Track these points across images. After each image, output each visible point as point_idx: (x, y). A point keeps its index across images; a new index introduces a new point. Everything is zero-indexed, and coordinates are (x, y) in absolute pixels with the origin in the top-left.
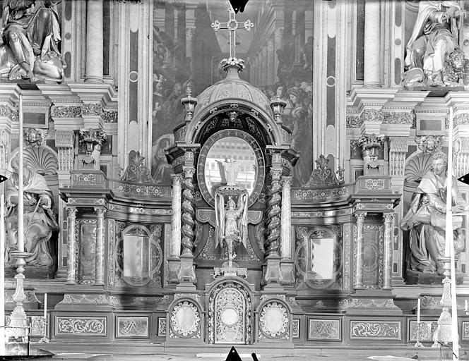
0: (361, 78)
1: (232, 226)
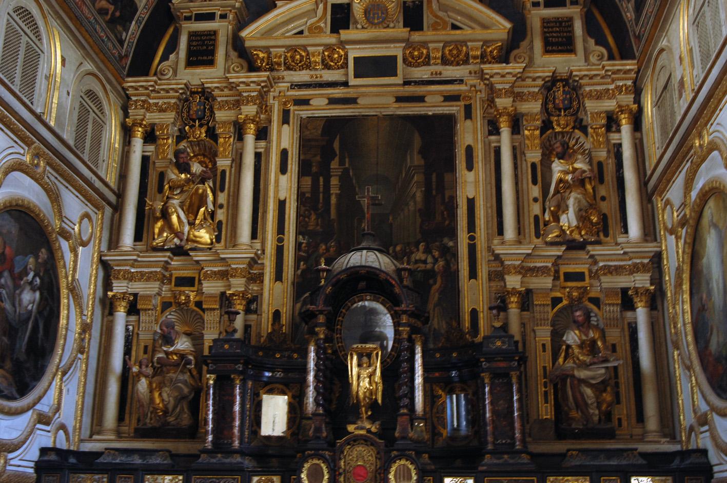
0: (501, 231)
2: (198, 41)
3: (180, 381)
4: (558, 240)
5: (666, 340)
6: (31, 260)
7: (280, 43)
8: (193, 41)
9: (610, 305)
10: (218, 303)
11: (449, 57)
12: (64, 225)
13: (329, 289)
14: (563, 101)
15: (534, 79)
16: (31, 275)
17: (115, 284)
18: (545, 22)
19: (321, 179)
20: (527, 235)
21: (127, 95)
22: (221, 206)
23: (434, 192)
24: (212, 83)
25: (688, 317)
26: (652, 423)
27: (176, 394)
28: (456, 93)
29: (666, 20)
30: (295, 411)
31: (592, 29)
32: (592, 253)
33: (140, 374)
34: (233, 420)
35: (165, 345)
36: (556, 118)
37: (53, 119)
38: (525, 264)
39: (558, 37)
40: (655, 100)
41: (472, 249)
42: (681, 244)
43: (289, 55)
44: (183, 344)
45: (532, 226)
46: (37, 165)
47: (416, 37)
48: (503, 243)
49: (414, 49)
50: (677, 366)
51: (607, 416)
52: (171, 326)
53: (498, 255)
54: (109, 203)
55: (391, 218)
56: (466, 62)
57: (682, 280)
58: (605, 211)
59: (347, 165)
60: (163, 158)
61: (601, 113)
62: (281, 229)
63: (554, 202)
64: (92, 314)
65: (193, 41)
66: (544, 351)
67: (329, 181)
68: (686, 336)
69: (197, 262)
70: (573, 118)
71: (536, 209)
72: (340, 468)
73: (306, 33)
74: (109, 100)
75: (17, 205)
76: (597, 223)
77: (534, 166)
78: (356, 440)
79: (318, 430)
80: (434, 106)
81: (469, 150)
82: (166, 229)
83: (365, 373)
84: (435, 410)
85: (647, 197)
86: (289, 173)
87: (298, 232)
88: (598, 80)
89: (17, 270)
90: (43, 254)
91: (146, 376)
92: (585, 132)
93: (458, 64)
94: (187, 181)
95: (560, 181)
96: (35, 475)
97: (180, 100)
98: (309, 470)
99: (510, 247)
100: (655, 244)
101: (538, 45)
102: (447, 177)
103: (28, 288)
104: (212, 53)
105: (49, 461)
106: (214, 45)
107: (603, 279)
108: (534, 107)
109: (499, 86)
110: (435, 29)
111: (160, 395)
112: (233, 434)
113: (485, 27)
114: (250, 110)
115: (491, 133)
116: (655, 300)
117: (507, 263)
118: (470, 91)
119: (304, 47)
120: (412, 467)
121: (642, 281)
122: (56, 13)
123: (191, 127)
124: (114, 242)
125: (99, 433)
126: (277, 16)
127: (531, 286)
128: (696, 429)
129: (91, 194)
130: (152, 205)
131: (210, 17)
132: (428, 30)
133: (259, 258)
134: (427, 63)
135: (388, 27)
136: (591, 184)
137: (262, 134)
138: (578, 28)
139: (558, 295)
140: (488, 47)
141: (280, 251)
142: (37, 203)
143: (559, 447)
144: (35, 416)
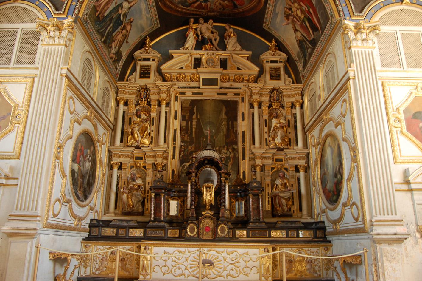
0: (254, 143)
2: (144, 69)
3: (138, 195)
4: (274, 147)
5: (310, 183)
6: (89, 151)
7: (175, 71)
8: (142, 69)
9: (291, 170)
10: (152, 167)
11: (236, 79)
12: (98, 138)
13: (197, 164)
14: (276, 97)
15: (267, 89)
16: (89, 156)
17: (113, 158)
18: (271, 68)
19: (189, 122)
20: (263, 145)
21: (117, 88)
22: (152, 131)
23: (230, 128)
24: (150, 85)
25: (319, 176)
26: (305, 212)
27: (137, 200)
28: (238, 93)
29: (314, 73)
30: (182, 207)
31: (287, 72)
32: (286, 152)
33: (123, 193)
34: (161, 210)
35: (133, 182)
36: (274, 103)
37: (96, 99)
38: (262, 156)
39: (275, 74)
40: (309, 99)
41: (244, 150)
42: (317, 151)
43: (178, 76)
44: (139, 182)
45: (265, 142)
46: (91, 116)
47: (225, 72)
48: (254, 148)
49: (224, 76)
50: (314, 193)
51: (290, 209)
52: (135, 175)
53: (253, 152)
54: (111, 129)
55: (214, 137)
56: (242, 82)
57: (318, 163)
58: (290, 137)
59: (199, 117)
60: (131, 112)
61: (290, 102)
62: (175, 140)
63: (273, 134)
64: (106, 170)
65: (142, 69)
66: (268, 186)
67: (192, 123)
68: (318, 183)
69: (144, 151)
70: (280, 104)
71: (266, 136)
72: (200, 227)
73: (184, 68)
74: (112, 90)
75: (86, 131)
76: (288, 142)
77: (266, 120)
78: (206, 217)
79: (192, 214)
80: (230, 97)
81: (243, 114)
82: (133, 139)
83: (208, 194)
84: (231, 207)
85: (305, 133)
86: (177, 120)
87: (181, 141)
88: (289, 90)
89: (85, 155)
90: (92, 148)
91: (126, 193)
92: (284, 109)
93: (239, 82)
94: (141, 121)
95: (275, 126)
96: (89, 229)
97: (137, 90)
98: (190, 228)
99: (257, 149)
100: (307, 150)
101: (268, 76)
102: (235, 123)
103: (88, 161)
104: (149, 73)
105: (94, 224)
106: (150, 71)
107: (289, 161)
108: (266, 99)
109: (254, 91)
110: (232, 69)
111: (131, 200)
112: (161, 215)
113: (250, 69)
114: (163, 96)
115: (250, 108)
116: (307, 169)
117: (256, 155)
118: (243, 92)
119: (184, 74)
120: (226, 227)
121: (303, 162)
122: (98, 60)
123: (141, 101)
124: (113, 143)
125: (107, 213)
126: (174, 61)
127: (264, 163)
128: (321, 214)
129: (106, 126)
130: (127, 130)
131: (148, 60)
132: (229, 69)
133: (167, 150)
134: (228, 81)
135: (215, 67)
136: (285, 127)
137: (168, 105)
138: (282, 71)
139: (273, 166)
140: (251, 77)
141: (174, 148)
142: (90, 129)
143: (274, 220)
144: (89, 208)
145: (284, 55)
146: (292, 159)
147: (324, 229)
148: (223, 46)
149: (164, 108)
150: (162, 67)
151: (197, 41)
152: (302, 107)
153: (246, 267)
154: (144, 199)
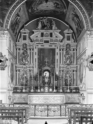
0: (60, 63)
1: (46, 81)
26: (75, 84)
47: (52, 38)
56: (57, 41)
80: (53, 47)
85: (77, 60)
104: (26, 38)
108: (65, 47)
114: (31, 47)
121: (75, 69)
124: (16, 64)
137: (33, 50)
145: (72, 31)
146: (72, 68)
147: (79, 89)
148: (51, 28)
149: (32, 51)
150: (30, 37)
151: (42, 25)
152: (76, 50)
153: (57, 99)
154: (27, 80)
